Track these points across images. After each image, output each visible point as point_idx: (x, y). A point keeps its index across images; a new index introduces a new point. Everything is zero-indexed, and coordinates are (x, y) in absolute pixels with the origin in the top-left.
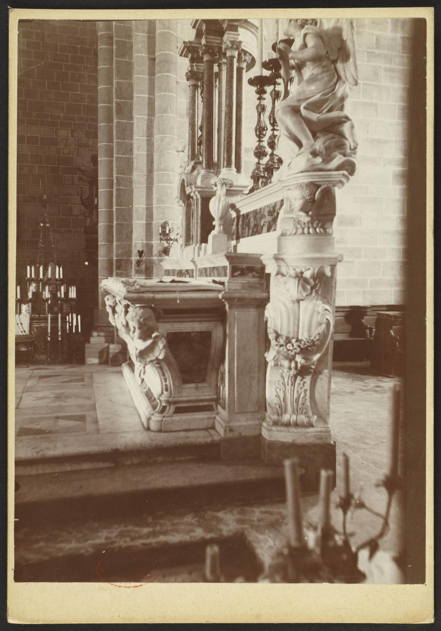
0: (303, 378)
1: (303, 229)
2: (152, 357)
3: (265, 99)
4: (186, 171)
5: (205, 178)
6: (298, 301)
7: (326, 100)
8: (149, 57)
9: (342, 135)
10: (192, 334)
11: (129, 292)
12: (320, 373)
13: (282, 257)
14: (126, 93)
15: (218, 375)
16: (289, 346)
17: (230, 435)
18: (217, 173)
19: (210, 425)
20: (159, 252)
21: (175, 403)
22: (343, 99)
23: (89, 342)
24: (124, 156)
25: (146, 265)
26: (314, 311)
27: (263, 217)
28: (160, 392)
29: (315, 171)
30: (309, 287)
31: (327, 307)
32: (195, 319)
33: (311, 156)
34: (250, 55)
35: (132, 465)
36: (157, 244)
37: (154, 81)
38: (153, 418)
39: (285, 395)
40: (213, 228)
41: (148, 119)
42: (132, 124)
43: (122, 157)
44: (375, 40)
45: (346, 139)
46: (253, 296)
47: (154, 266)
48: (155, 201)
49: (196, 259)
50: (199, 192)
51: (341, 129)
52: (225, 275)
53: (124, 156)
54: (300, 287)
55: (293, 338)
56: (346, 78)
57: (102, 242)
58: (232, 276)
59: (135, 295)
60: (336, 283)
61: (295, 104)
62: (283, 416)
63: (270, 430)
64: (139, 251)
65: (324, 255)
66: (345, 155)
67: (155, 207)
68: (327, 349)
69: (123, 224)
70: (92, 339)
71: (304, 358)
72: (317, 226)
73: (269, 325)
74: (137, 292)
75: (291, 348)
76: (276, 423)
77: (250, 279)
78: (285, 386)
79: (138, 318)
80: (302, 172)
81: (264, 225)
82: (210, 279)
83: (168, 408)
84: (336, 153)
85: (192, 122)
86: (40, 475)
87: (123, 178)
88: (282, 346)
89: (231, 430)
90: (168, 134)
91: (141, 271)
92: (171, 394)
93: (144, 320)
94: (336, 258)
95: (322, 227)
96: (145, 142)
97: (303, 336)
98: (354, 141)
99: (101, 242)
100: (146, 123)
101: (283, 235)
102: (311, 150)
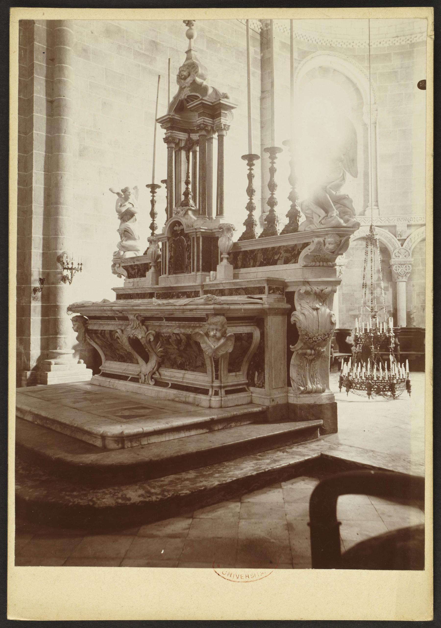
3: (248, 169)
10: (243, 335)
19: (249, 401)
35: (219, 430)
81: (278, 259)
91: (37, 298)
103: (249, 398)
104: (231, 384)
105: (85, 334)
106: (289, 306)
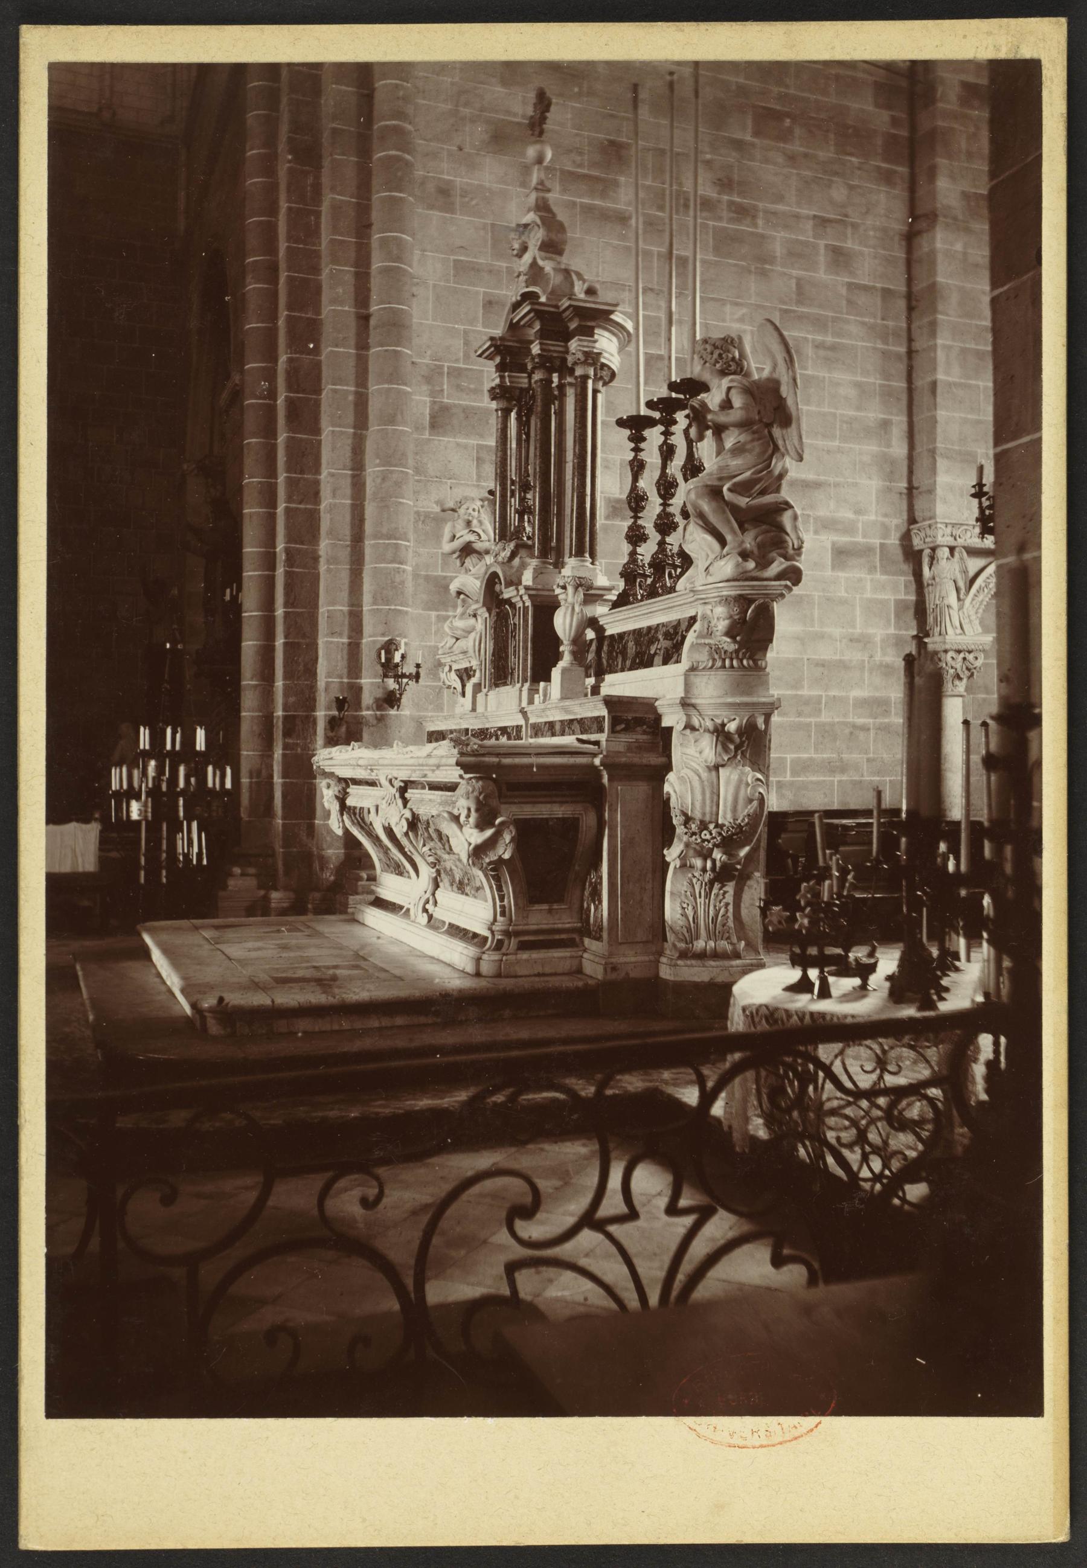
0: (723, 886)
1: (724, 660)
2: (492, 857)
4: (500, 559)
5: (538, 573)
6: (717, 767)
7: (759, 480)
8: (357, 313)
9: (781, 529)
11: (462, 754)
12: (749, 877)
13: (693, 701)
14: (307, 381)
15: (584, 889)
16: (705, 835)
17: (613, 976)
18: (559, 565)
19: (574, 968)
20: (377, 700)
21: (517, 934)
22: (781, 476)
23: (225, 887)
24: (302, 506)
25: (347, 728)
26: (740, 781)
27: (653, 640)
28: (491, 918)
29: (746, 580)
30: (732, 747)
31: (759, 776)
32: (555, 799)
33: (740, 559)
34: (609, 368)
36: (370, 682)
37: (367, 361)
38: (485, 957)
39: (695, 913)
40: (557, 657)
41: (355, 434)
42: (319, 442)
43: (297, 509)
44: (794, 286)
45: (787, 534)
46: (645, 761)
47: (365, 729)
48: (367, 598)
49: (529, 709)
50: (530, 596)
51: (778, 519)
52: (601, 730)
53: (302, 506)
54: (719, 747)
55: (710, 822)
56: (787, 450)
57: (252, 679)
58: (613, 730)
59: (472, 759)
60: (770, 741)
61: (716, 483)
62: (695, 943)
63: (676, 965)
64: (337, 699)
65: (755, 699)
66: (786, 558)
67: (369, 611)
68: (759, 840)
69: (298, 643)
70: (231, 883)
71: (725, 853)
72: (744, 657)
73: (673, 802)
74: (474, 754)
75: (708, 837)
76: (684, 955)
77: (640, 736)
78: (695, 899)
79: (476, 793)
80: (728, 581)
81: (655, 653)
82: (574, 737)
83: (506, 942)
84: (774, 554)
85: (501, 472)
86: (337, 1031)
87: (299, 551)
88: (694, 834)
89: (614, 969)
90: (395, 466)
92: (511, 920)
93: (485, 797)
94: (772, 704)
95: (750, 658)
96: (349, 480)
97: (725, 817)
98: (799, 538)
99: (248, 680)
100: (350, 441)
101: (693, 669)
102: (740, 549)
103: (576, 962)
104: (535, 927)
105: (342, 815)
106: (663, 760)
